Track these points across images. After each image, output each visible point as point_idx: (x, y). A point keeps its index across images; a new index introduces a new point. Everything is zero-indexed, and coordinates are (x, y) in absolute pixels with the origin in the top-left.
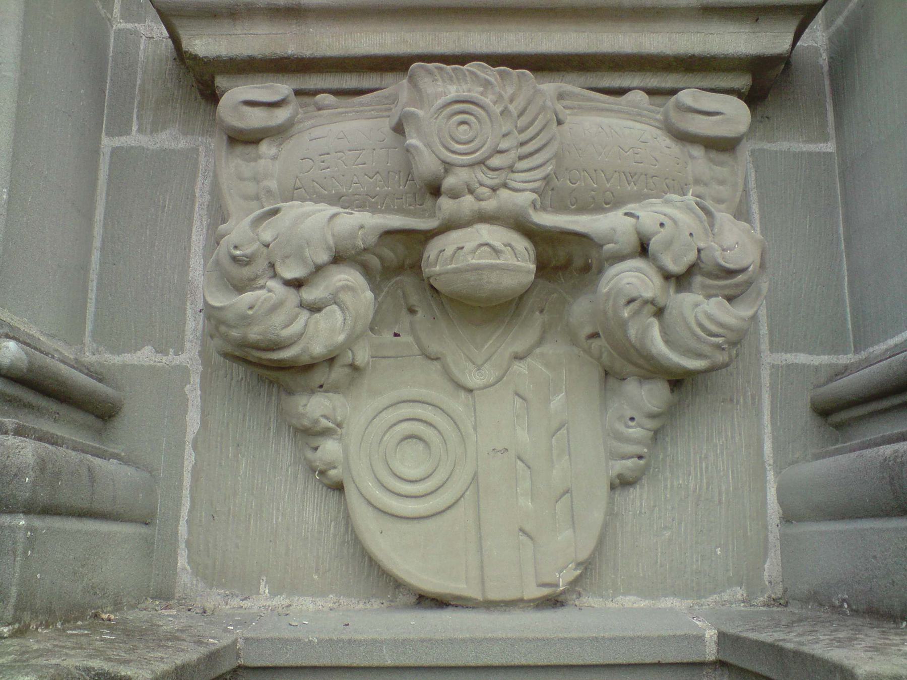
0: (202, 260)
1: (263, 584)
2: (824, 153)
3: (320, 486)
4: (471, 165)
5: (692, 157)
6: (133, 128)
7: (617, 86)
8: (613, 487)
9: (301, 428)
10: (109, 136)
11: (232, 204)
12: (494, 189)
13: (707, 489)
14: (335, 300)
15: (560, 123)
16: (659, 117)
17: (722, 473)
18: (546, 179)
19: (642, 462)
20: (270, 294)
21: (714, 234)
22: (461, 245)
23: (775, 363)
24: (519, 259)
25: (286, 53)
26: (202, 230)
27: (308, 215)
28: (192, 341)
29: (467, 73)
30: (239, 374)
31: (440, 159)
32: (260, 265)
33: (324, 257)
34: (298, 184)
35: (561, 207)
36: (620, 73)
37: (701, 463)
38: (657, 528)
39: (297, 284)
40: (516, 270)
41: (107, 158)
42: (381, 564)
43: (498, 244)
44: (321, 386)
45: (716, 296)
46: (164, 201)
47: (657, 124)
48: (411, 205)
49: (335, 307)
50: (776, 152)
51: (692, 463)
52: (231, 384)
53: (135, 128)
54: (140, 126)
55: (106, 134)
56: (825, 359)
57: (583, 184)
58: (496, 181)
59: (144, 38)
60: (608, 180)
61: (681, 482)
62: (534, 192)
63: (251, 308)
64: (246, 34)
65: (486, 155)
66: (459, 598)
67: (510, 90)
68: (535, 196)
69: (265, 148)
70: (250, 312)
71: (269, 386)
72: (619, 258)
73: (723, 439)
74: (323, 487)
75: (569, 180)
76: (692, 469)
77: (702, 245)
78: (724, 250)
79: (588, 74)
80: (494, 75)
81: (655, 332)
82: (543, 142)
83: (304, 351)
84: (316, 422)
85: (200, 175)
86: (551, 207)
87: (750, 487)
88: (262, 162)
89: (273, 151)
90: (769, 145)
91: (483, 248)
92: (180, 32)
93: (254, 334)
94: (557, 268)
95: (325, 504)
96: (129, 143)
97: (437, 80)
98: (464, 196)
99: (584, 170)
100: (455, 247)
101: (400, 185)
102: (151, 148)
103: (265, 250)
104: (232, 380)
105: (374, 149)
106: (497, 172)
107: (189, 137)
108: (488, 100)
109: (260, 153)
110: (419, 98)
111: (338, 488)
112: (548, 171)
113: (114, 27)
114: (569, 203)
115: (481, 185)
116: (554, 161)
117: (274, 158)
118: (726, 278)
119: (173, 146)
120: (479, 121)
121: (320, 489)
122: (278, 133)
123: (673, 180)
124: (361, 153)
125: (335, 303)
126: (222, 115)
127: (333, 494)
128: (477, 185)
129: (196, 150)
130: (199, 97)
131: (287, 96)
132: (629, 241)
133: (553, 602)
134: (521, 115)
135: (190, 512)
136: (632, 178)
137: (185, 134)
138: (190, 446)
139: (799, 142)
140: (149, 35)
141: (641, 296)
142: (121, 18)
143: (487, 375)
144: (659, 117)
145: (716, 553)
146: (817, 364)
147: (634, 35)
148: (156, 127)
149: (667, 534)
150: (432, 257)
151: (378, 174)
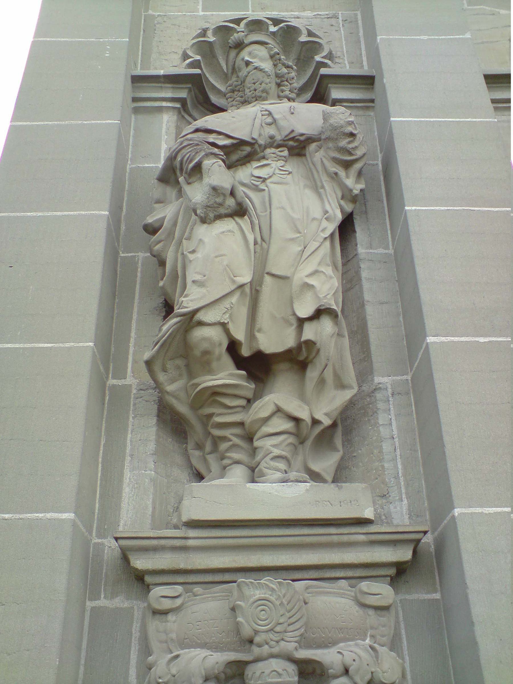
2: (435, 599)
4: (267, 631)
5: (369, 615)
6: (102, 596)
7: (333, 576)
10: (90, 601)
11: (155, 645)
12: (277, 642)
15: (306, 603)
16: (353, 594)
18: (302, 635)
21: (378, 663)
22: (263, 671)
24: (290, 677)
25: (179, 568)
26: (135, 652)
27: (192, 658)
29: (264, 585)
31: (252, 629)
34: (186, 637)
35: (309, 646)
36: (335, 570)
41: (89, 612)
43: (280, 671)
46: (117, 636)
47: (352, 598)
48: (239, 647)
50: (412, 600)
53: (102, 596)
54: (105, 594)
55: (88, 600)
57: (318, 635)
58: (278, 638)
59: (107, 547)
60: (330, 633)
62: (296, 642)
64: (161, 558)
67: (283, 591)
69: (171, 617)
72: (336, 677)
75: (312, 633)
77: (373, 670)
78: (384, 673)
79: (320, 571)
80: (276, 584)
82: (299, 617)
86: (304, 646)
88: (169, 624)
89: (174, 618)
90: (409, 596)
91: (274, 673)
92: (130, 557)
94: (308, 674)
96: (99, 604)
97: (250, 588)
98: (263, 646)
99: (319, 628)
101: (234, 638)
102: (110, 607)
103: (173, 678)
105: (222, 620)
106: (278, 634)
107: (130, 601)
108: (273, 598)
109: (168, 619)
110: (242, 597)
112: (302, 632)
113: (93, 542)
115: (272, 640)
116: (304, 627)
117: (174, 622)
119: (122, 606)
120: (270, 610)
123: (360, 629)
128: (270, 641)
129: (132, 608)
130: (134, 579)
131: (182, 593)
132: (340, 669)
134: (288, 603)
136: (341, 630)
137: (128, 599)
139: (423, 594)
140: (110, 546)
142: (96, 537)
144: (353, 594)
147: (339, 554)
148: (113, 595)
150: (250, 676)
151: (224, 633)
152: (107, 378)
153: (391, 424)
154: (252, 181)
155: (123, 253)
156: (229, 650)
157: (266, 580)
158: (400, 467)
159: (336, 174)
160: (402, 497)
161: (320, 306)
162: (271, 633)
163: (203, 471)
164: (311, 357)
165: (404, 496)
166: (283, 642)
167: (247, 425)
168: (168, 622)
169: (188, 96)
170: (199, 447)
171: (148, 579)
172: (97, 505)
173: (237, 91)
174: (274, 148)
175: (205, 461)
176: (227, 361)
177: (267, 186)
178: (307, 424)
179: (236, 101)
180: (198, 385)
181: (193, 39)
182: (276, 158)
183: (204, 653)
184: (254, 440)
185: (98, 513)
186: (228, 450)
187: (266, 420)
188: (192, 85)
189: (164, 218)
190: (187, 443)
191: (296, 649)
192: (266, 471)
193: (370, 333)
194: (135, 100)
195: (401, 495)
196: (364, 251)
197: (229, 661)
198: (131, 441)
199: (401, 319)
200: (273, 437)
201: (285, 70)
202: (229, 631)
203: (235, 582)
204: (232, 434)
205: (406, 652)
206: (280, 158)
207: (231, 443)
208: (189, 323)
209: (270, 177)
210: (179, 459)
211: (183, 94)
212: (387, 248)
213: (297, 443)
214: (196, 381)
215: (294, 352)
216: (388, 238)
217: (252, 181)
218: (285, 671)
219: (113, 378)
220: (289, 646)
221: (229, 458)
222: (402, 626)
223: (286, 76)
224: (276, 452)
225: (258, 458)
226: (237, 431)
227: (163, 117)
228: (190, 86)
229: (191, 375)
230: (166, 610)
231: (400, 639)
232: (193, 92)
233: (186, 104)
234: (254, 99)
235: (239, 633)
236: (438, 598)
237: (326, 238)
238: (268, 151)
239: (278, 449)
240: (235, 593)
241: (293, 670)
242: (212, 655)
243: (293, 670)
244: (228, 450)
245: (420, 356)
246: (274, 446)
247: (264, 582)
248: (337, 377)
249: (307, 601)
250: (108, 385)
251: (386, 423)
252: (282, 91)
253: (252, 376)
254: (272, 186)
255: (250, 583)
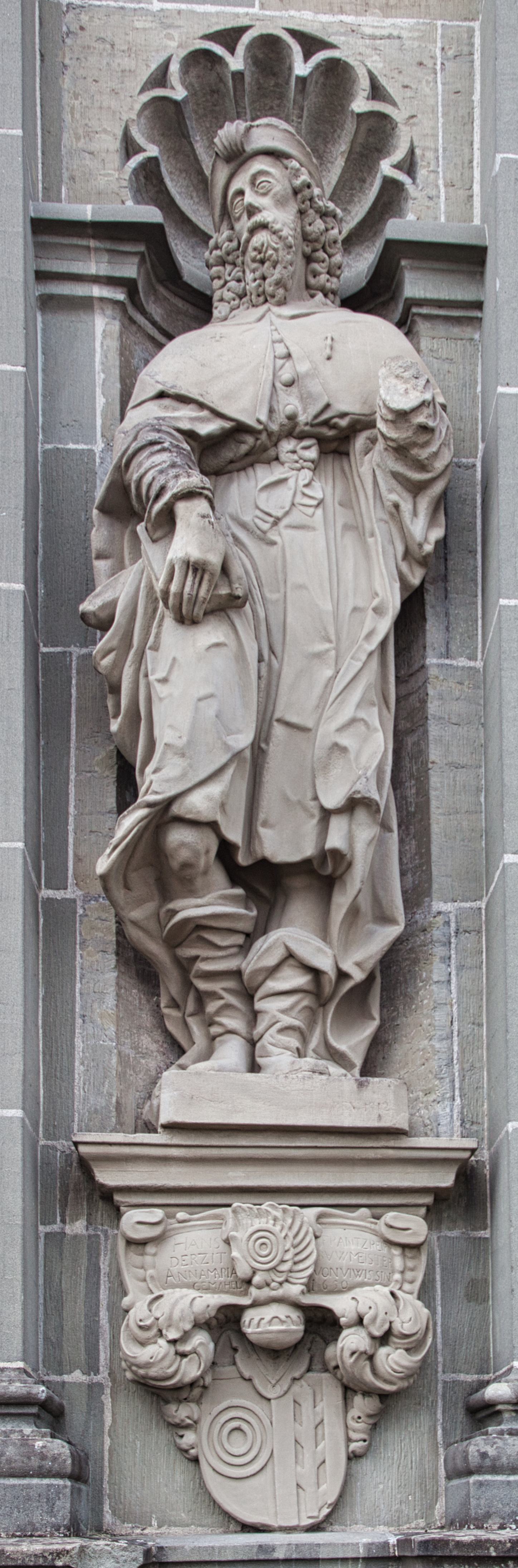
1: (153, 1520)
4: (268, 1270)
8: (349, 1459)
12: (281, 1284)
14: (194, 1351)
18: (311, 1277)
19: (366, 1443)
33: (188, 1326)
39: (174, 1342)
40: (294, 1332)
43: (283, 1317)
44: (185, 1399)
49: (195, 1355)
56: (475, 1377)
63: (151, 1358)
66: (264, 1525)
69: (150, 1249)
70: (152, 1361)
83: (180, 1381)
84: (183, 1421)
93: (153, 1372)
111: (196, 1460)
116: (313, 1266)
122: (157, 1240)
132: (353, 1316)
133: (315, 1528)
143: (279, 1390)
146: (470, 1380)
149: (381, 1486)
150: (247, 1323)
152: (40, 888)
153: (449, 981)
154: (257, 521)
155: (45, 646)
156: (227, 1292)
157: (267, 1204)
158: (456, 1048)
159: (397, 506)
160: (454, 1095)
161: (354, 793)
163: (183, 1042)
164: (339, 872)
165: (457, 1093)
167: (245, 977)
168: (146, 1254)
169: (139, 273)
170: (174, 1004)
172: (42, 1092)
173: (230, 264)
174: (295, 438)
175: (186, 1024)
176: (218, 876)
177: (280, 534)
178: (330, 979)
179: (228, 290)
180: (174, 912)
181: (143, 90)
182: (297, 462)
183: (193, 1293)
184: (256, 999)
185: (44, 1103)
186: (218, 1012)
187: (272, 971)
188: (148, 248)
189: (113, 604)
190: (159, 995)
191: (303, 1292)
192: (271, 1048)
193: (433, 821)
194: (42, 276)
195: (454, 1091)
196: (434, 661)
198: (81, 994)
199: (482, 800)
200: (282, 998)
201: (319, 225)
203: (229, 1206)
204: (224, 989)
205: (439, 1302)
206: (305, 464)
207: (221, 1002)
208: (162, 816)
209: (287, 513)
210: (146, 1019)
211: (129, 270)
212: (472, 657)
213: (314, 1006)
214: (171, 906)
215: (315, 863)
216: (477, 635)
217: (257, 521)
219: (48, 887)
220: (294, 1290)
221: (220, 1024)
222: (438, 1270)
223: (323, 239)
224: (287, 1020)
225: (260, 1028)
226: (231, 984)
227: (94, 321)
228: (142, 248)
229: (165, 893)
230: (144, 1239)
231: (434, 1287)
232: (149, 265)
233: (136, 291)
234: (261, 299)
236: (487, 1236)
237: (371, 654)
238: (287, 445)
239: (288, 1015)
240: (230, 1222)
244: (218, 1012)
245: (496, 879)
246: (284, 1011)
248: (377, 901)
249: (318, 1234)
250: (40, 899)
251: (443, 979)
252: (315, 274)
253: (252, 896)
254: (288, 534)
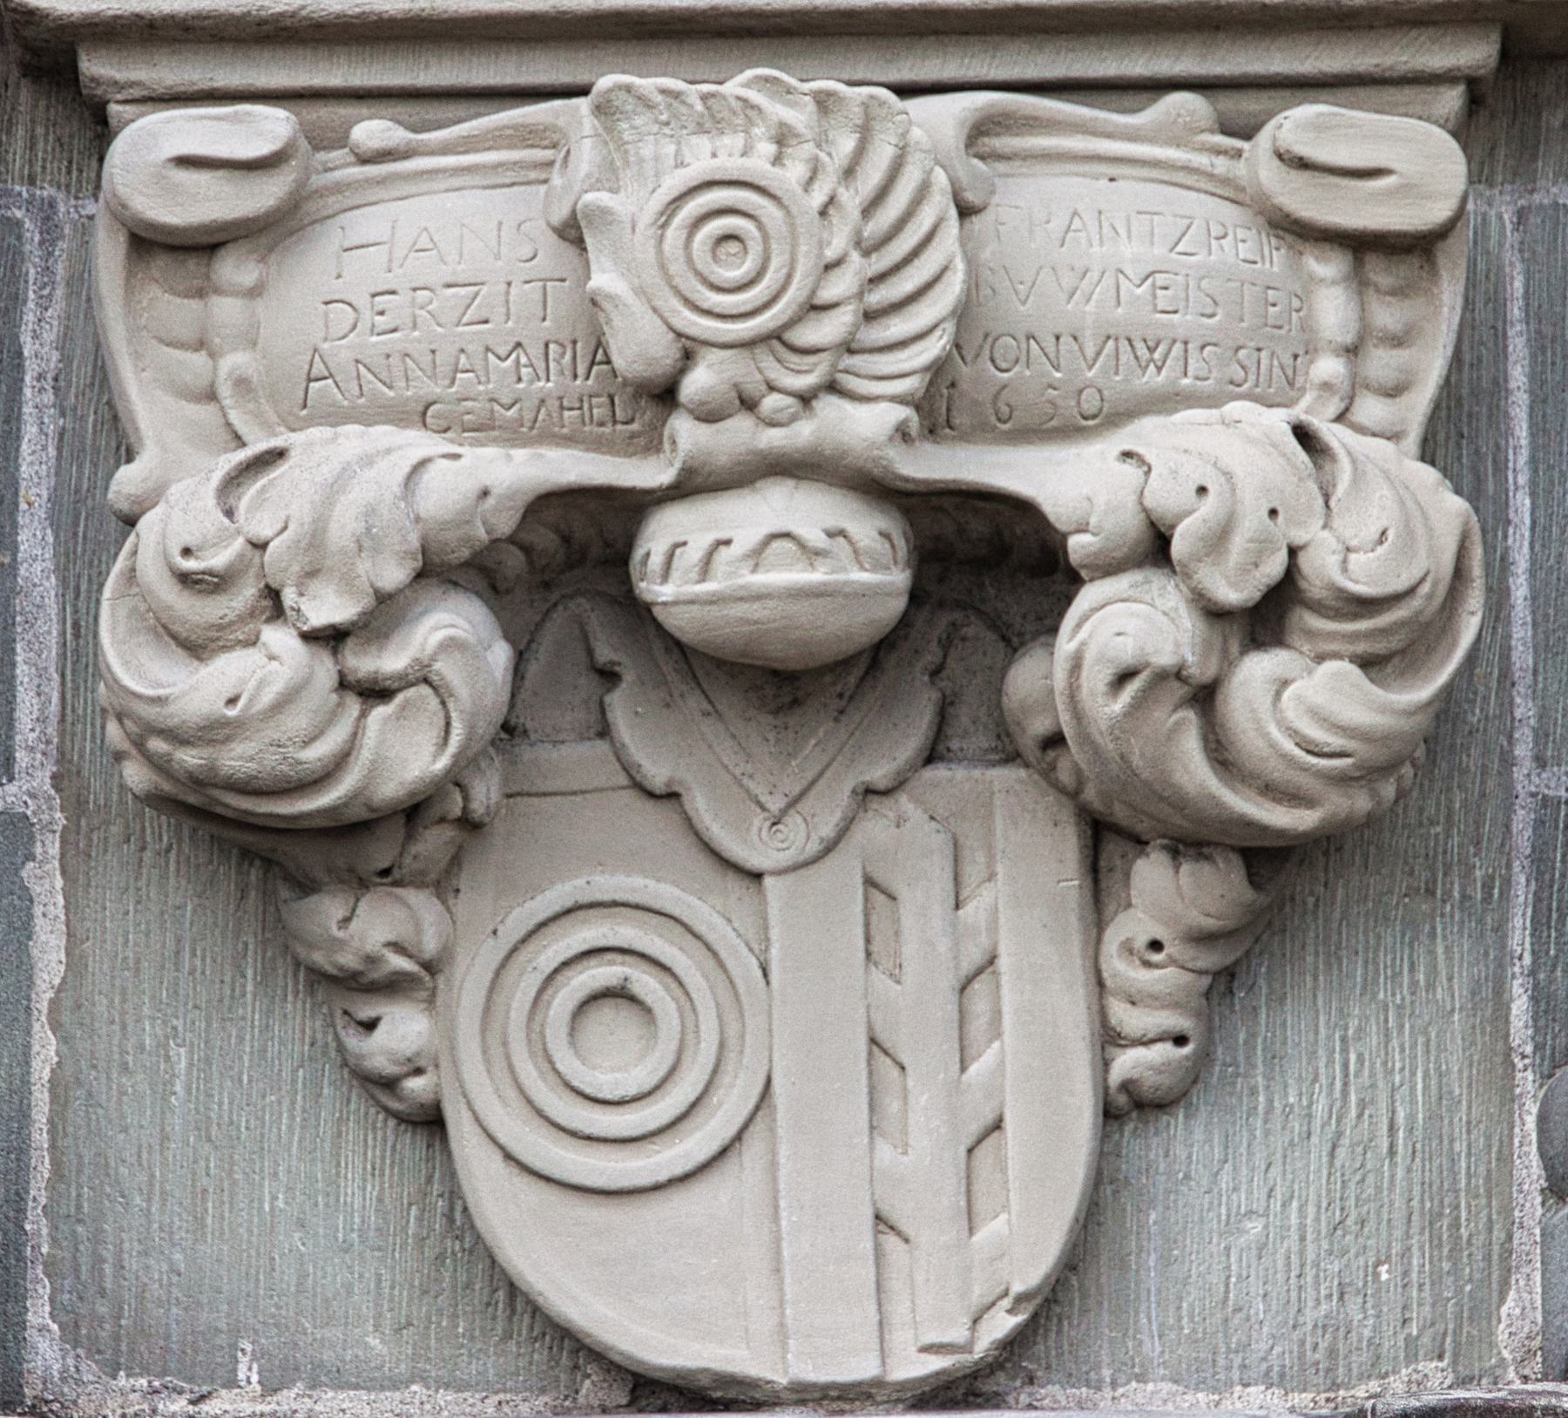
0: (49, 531)
3: (381, 1117)
8: (1110, 1114)
9: (334, 972)
13: (1360, 1116)
14: (422, 676)
17: (1397, 1079)
18: (938, 370)
19: (1187, 1050)
20: (275, 664)
23: (1551, 793)
26: (44, 448)
28: (32, 749)
30: (160, 835)
31: (671, 329)
32: (246, 594)
33: (394, 575)
37: (1345, 1051)
38: (1229, 1216)
39: (331, 638)
42: (541, 1300)
44: (385, 872)
45: (1336, 656)
51: (1321, 1052)
52: (141, 860)
61: (1291, 1100)
63: (232, 701)
65: (785, 318)
68: (903, 412)
69: (235, 269)
70: (232, 713)
71: (239, 865)
73: (1405, 991)
74: (385, 1121)
76: (1322, 1064)
81: (1191, 745)
83: (355, 796)
85: (31, 295)
87: (1469, 1114)
91: (777, 545)
93: (237, 759)
95: (393, 1162)
100: (709, 539)
104: (143, 849)
108: (758, 164)
114: (993, 419)
116: (950, 327)
118: (1356, 616)
121: (379, 1125)
124: (476, 295)
125: (426, 681)
126: (121, 190)
127: (413, 1143)
132: (1125, 525)
135: (51, 1186)
138: (44, 1019)
141: (1147, 665)
143: (798, 838)
145: (1376, 1275)
150: (656, 561)
151: (520, 350)
162: (773, 353)
166: (833, 400)
168: (218, 291)
171: (95, 66)
183: (417, 443)
197: (542, 490)
202: (547, 346)
203: (583, 91)
218: (841, 540)
235: (600, 351)
240: (586, 155)
241: (881, 534)
242: (457, 457)
243: (885, 535)
247: (744, 92)
255: (659, 98)
